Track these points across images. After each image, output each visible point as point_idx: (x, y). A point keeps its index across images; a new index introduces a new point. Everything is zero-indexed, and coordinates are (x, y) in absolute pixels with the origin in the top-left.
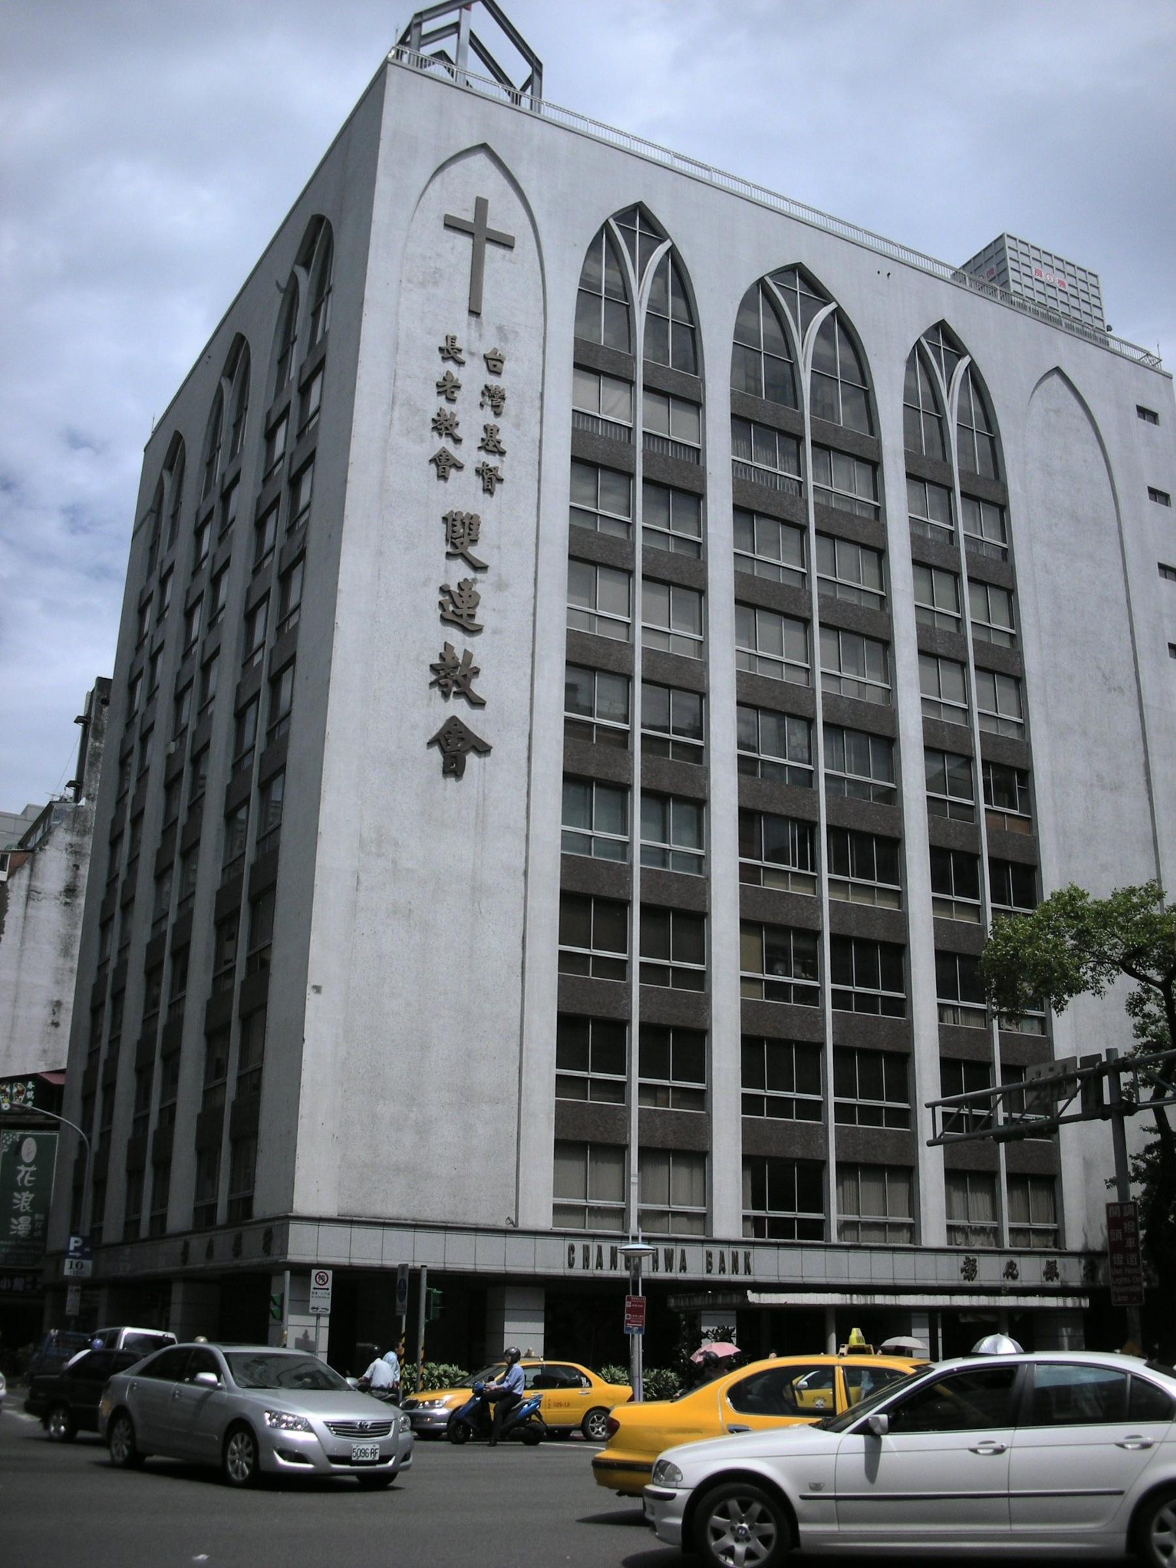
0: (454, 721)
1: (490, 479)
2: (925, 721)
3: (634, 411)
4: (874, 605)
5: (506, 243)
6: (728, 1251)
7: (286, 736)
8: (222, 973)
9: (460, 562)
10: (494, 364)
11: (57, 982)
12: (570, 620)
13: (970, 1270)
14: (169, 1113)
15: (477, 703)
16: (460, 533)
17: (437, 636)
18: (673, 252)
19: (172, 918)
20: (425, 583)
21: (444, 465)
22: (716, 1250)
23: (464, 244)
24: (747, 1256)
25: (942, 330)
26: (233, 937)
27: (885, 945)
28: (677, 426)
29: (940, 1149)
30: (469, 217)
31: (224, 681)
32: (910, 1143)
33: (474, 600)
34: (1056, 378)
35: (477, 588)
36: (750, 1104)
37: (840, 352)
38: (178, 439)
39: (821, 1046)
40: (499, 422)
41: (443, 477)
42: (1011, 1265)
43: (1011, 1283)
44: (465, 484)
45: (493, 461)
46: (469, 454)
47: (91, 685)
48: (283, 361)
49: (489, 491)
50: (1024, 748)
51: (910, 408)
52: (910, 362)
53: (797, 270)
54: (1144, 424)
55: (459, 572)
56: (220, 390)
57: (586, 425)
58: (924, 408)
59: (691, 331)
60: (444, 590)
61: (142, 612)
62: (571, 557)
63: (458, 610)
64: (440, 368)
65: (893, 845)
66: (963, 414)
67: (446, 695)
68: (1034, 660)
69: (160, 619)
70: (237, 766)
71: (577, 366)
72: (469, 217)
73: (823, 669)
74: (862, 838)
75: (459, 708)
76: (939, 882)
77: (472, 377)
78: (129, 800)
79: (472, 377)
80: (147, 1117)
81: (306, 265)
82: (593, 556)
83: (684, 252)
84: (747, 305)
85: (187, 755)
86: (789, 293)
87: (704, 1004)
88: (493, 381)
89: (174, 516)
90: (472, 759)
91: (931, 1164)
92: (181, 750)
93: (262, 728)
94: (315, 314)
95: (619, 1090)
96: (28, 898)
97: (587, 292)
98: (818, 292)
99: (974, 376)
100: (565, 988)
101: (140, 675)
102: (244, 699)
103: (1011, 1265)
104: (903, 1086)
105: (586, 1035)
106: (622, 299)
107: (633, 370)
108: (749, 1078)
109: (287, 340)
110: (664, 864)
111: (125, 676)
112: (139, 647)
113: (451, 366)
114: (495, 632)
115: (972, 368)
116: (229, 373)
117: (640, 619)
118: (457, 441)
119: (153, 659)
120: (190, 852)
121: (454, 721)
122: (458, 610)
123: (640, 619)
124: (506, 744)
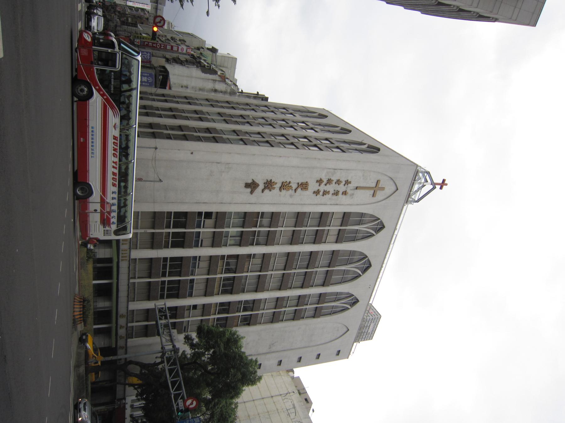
0: (258, 185)
1: (317, 193)
2: (261, 299)
3: (333, 228)
4: (311, 284)
5: (374, 195)
6: (127, 255)
7: (254, 145)
8: (195, 129)
9: (297, 186)
10: (345, 193)
11: (193, 87)
12: (283, 213)
13: (122, 316)
14: (160, 116)
15: (263, 191)
16: (304, 186)
17: (278, 181)
18: (373, 235)
19: (209, 117)
20: (291, 178)
21: (320, 181)
22: (128, 252)
23: (374, 185)
24: (126, 260)
25: (357, 301)
26: (206, 132)
27: (178, 294)
28: (332, 237)
29: (154, 307)
30: (380, 186)
31: (267, 129)
32: (155, 299)
33: (288, 190)
34: (345, 330)
35: (291, 191)
36: (165, 259)
37: (350, 276)
38: (326, 117)
39: (180, 276)
40: (330, 195)
41: (317, 181)
42: (123, 327)
43: (119, 327)
44: (315, 187)
45: (321, 193)
46: (322, 188)
47: (266, 96)
48: (345, 142)
49: (314, 192)
50: (255, 324)
51: (337, 294)
52: (348, 293)
53: (370, 266)
54: (336, 352)
55: (294, 186)
56: (337, 127)
57: (330, 216)
58: (337, 297)
59: (354, 239)
60: (290, 182)
61: (284, 108)
62: (298, 213)
63: (285, 186)
64: (343, 180)
65: (231, 292)
66: (337, 307)
67: (264, 183)
68: (277, 326)
69: (282, 113)
70: (247, 133)
71: (345, 213)
72: (380, 186)
73: (274, 274)
74: (232, 285)
75: (261, 186)
76: (222, 304)
77: (341, 188)
78: (238, 106)
79: (341, 188)
80: (167, 130)
81: (368, 147)
82: (300, 218)
83: (373, 238)
84: (361, 254)
85: (249, 120)
86: (364, 263)
87: (190, 247)
88: (340, 193)
89: (307, 116)
90: (249, 190)
91: (150, 305)
92: (250, 119)
93: (256, 139)
94: (356, 150)
95: (168, 227)
96: (214, 80)
97: (362, 215)
98: (365, 270)
99: (346, 309)
100: (193, 213)
101: (266, 121)
102: (263, 134)
103: (123, 327)
104: (170, 296)
105: (182, 219)
106: (360, 223)
107: (344, 226)
108: (172, 259)
109: (350, 143)
110: (225, 237)
111: (269, 104)
112: (275, 108)
113: (344, 183)
114: (280, 195)
115: (348, 309)
116: (342, 129)
117: (284, 229)
118: (326, 185)
119: (272, 112)
120: (226, 122)
121: (258, 185)
122: (285, 186)
123: (284, 229)
124: (253, 198)
